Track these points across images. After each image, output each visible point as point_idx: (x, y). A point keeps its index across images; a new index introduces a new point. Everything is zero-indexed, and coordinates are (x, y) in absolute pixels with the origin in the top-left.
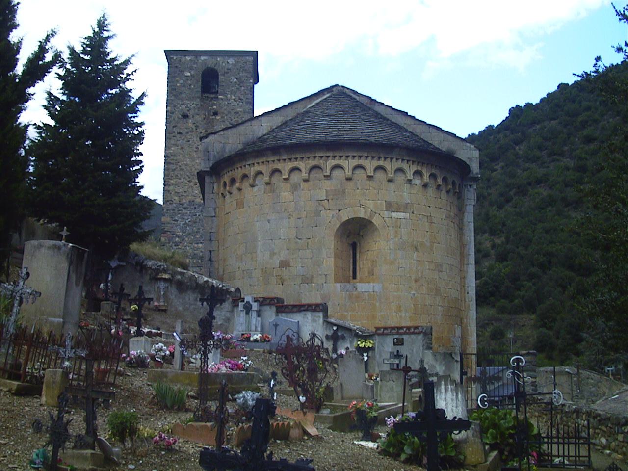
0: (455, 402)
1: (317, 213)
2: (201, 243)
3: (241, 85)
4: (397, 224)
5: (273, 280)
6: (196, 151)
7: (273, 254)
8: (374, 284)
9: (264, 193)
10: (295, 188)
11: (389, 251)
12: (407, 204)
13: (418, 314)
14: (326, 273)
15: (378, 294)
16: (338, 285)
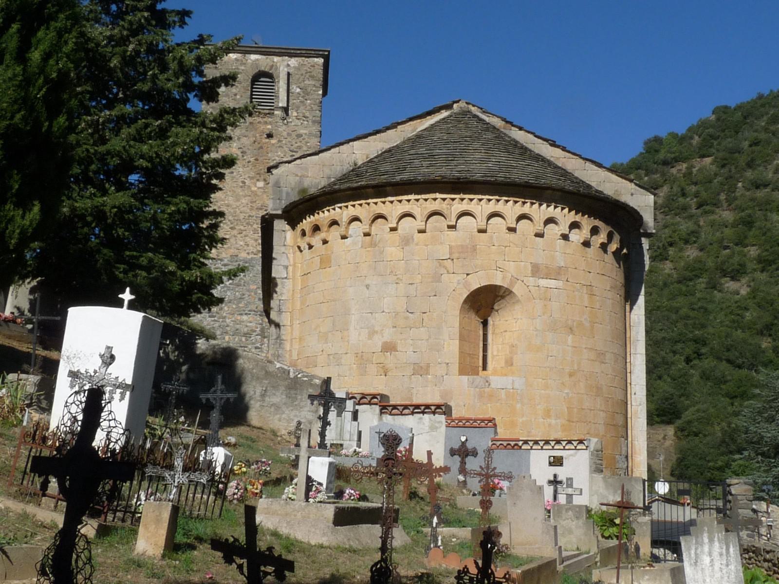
0: (725, 557)
1: (437, 278)
2: (246, 314)
3: (307, 97)
4: (546, 297)
5: (372, 369)
6: (241, 187)
7: (372, 333)
8: (515, 379)
9: (362, 247)
10: (406, 241)
11: (535, 333)
12: (560, 268)
13: (573, 422)
14: (448, 362)
15: (519, 392)
16: (465, 378)
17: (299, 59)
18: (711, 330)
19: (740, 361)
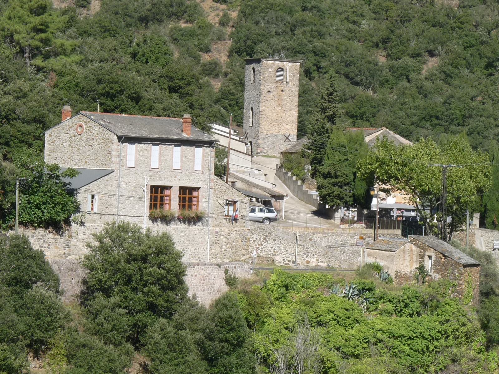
17: (292, 63)
18: (329, 40)
19: (358, 79)
